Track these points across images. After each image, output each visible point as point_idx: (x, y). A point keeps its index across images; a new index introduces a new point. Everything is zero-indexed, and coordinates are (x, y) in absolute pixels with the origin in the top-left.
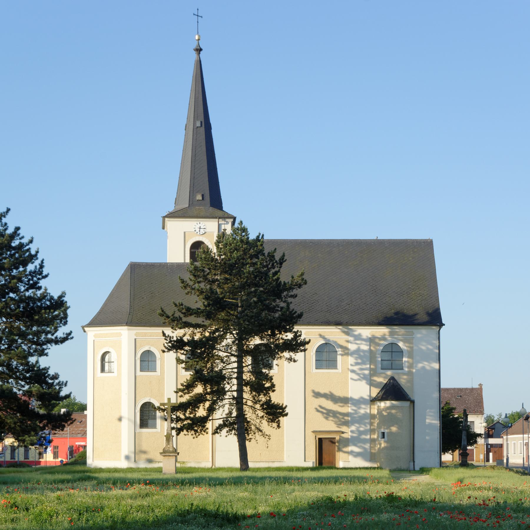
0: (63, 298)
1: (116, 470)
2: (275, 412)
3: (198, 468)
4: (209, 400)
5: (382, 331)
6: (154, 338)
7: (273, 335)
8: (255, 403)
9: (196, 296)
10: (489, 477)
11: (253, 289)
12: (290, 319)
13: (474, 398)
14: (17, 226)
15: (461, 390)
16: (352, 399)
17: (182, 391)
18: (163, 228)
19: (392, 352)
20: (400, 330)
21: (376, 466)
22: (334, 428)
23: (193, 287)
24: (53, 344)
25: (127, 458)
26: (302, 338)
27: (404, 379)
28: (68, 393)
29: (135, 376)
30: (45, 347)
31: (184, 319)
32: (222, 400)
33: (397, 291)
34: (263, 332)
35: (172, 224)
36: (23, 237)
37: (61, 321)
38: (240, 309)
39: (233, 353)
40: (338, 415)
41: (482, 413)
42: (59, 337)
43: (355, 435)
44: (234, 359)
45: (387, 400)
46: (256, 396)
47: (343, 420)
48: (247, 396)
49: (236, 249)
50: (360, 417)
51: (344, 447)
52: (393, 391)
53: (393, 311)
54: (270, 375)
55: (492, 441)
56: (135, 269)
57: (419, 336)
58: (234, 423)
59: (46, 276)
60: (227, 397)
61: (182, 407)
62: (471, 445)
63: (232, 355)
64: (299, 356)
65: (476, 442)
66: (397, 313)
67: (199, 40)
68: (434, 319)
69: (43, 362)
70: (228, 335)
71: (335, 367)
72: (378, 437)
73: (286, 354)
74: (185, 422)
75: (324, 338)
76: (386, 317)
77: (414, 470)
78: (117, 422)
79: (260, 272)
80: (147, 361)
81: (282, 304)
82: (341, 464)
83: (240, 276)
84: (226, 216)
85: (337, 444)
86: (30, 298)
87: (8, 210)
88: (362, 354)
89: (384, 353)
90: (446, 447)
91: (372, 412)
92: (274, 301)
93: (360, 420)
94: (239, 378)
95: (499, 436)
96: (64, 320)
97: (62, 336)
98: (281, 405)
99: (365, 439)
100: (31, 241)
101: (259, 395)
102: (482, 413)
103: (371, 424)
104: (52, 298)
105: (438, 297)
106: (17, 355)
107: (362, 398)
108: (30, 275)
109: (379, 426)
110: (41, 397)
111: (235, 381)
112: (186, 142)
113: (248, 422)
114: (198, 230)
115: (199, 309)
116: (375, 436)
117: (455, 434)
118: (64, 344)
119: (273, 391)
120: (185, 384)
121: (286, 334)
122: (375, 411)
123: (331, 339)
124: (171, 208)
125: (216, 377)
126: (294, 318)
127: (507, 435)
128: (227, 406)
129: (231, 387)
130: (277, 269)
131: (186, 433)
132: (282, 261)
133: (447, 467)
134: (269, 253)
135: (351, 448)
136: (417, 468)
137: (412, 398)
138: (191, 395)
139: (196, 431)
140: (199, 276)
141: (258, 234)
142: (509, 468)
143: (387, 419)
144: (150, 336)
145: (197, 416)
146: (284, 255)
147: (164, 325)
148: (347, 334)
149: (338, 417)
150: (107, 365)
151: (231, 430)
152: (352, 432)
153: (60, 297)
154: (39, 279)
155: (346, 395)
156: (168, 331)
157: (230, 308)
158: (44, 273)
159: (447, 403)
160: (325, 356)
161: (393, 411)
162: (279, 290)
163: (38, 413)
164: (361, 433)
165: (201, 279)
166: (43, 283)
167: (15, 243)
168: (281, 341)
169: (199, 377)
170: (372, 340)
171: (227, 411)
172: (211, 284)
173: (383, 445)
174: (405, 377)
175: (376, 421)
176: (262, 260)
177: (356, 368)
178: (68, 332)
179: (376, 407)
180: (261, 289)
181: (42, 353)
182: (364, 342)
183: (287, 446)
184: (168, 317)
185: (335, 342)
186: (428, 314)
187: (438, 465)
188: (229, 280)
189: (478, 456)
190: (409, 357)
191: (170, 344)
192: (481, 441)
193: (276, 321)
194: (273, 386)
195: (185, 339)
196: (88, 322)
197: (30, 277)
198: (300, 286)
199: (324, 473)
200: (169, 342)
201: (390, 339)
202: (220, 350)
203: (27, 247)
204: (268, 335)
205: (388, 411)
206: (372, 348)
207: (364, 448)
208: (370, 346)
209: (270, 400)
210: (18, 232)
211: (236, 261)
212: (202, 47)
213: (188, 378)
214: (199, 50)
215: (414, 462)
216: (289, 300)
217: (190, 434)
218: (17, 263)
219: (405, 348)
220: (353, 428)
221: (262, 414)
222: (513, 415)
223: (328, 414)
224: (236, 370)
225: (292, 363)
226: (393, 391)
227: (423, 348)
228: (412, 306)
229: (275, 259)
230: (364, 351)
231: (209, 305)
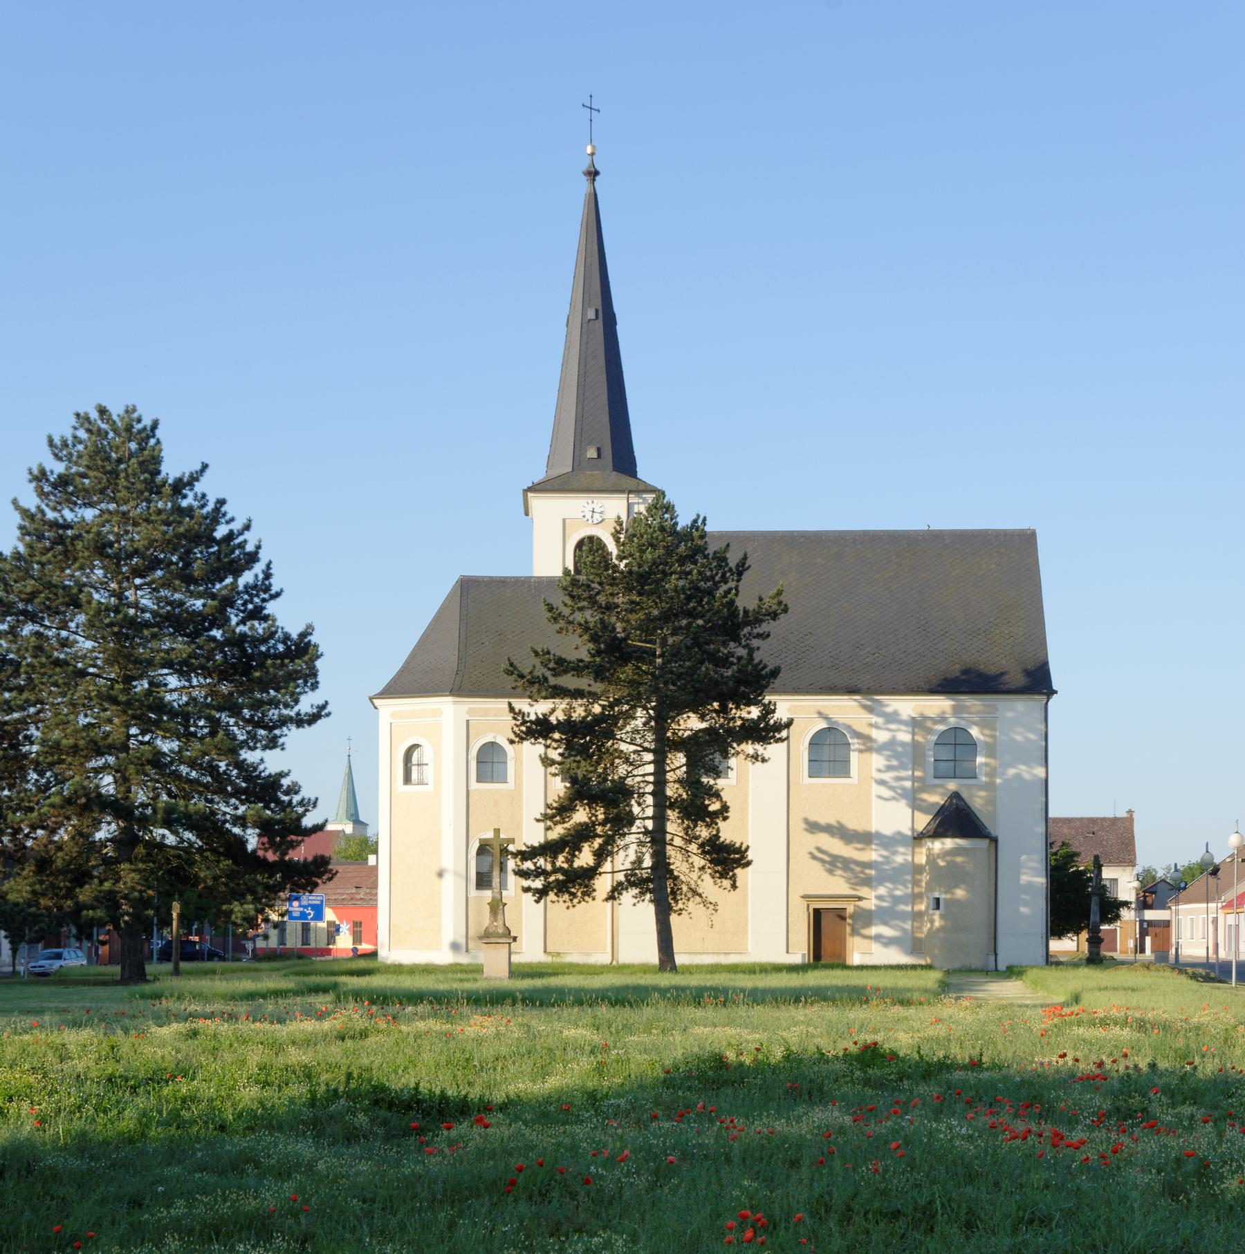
0: (309, 638)
1: (428, 970)
2: (727, 860)
3: (584, 965)
4: (600, 836)
5: (938, 705)
6: (493, 717)
7: (724, 710)
8: (690, 842)
9: (576, 636)
10: (1133, 990)
11: (684, 622)
12: (755, 682)
13: (1117, 837)
14: (221, 496)
15: (1093, 821)
16: (878, 835)
17: (551, 818)
18: (527, 514)
19: (957, 744)
20: (973, 703)
21: (923, 962)
22: (845, 889)
23: (571, 619)
24: (293, 727)
25: (455, 947)
26: (777, 716)
27: (980, 797)
28: (320, 821)
29: (468, 791)
30: (277, 732)
31: (553, 681)
32: (624, 835)
33: (965, 625)
34: (704, 704)
35: (542, 504)
36: (232, 520)
37: (306, 682)
38: (659, 661)
39: (646, 745)
40: (852, 866)
41: (1132, 863)
42: (303, 712)
43: (885, 904)
44: (649, 757)
45: (946, 836)
46: (689, 827)
47: (862, 875)
48: (674, 827)
49: (651, 545)
50: (894, 869)
51: (863, 928)
52: (957, 820)
53: (958, 666)
54: (719, 787)
55: (1150, 915)
56: (468, 587)
57: (1009, 715)
58: (648, 880)
59: (278, 595)
60: (634, 829)
61: (550, 849)
62: (1110, 921)
63: (646, 750)
64: (774, 751)
65: (1117, 917)
66: (966, 672)
67: (593, 154)
68: (1038, 682)
69: (270, 762)
70: (640, 712)
71: (845, 773)
72: (927, 908)
73: (749, 748)
74: (552, 878)
75: (827, 718)
76: (945, 679)
77: (996, 970)
78: (434, 878)
79: (697, 589)
80: (489, 762)
81: (741, 652)
82: (856, 959)
83: (659, 597)
84: (642, 487)
85: (849, 921)
86: (243, 636)
87: (205, 467)
88: (900, 749)
89: (940, 747)
90: (1057, 928)
91: (916, 861)
92: (725, 644)
93: (895, 876)
94: (659, 793)
95: (1163, 906)
96: (310, 677)
97: (309, 710)
98: (737, 845)
99: (904, 912)
100: (247, 527)
101: (696, 826)
102: (1132, 863)
103: (916, 883)
104: (287, 637)
105: (1045, 639)
106: (216, 747)
107: (899, 833)
108: (247, 592)
109: (930, 888)
110: (266, 828)
111: (649, 800)
112: (567, 348)
113: (676, 878)
114: (589, 515)
115: (581, 661)
116: (923, 907)
117: (1076, 900)
118: (314, 726)
119: (725, 819)
120: (555, 805)
121: (748, 709)
122: (921, 859)
123: (841, 721)
124: (539, 475)
125: (610, 790)
126: (763, 678)
127: (1177, 903)
128: (633, 847)
129: (643, 810)
130: (732, 584)
131: (555, 898)
132: (742, 568)
133: (1058, 964)
134: (715, 553)
135: (874, 930)
136: (1002, 966)
137: (993, 834)
138: (567, 825)
139: (574, 895)
140: (579, 598)
141: (694, 517)
142: (1180, 967)
143: (946, 875)
144: (496, 715)
145: (576, 865)
146: (745, 558)
147: (513, 693)
148: (870, 710)
149: (852, 870)
150: (414, 769)
151: (642, 893)
152: (879, 898)
153: (303, 635)
154: (264, 600)
155: (867, 829)
156: (522, 704)
157: (640, 659)
158: (274, 589)
159: (1064, 844)
160: (826, 752)
161: (959, 859)
162: (733, 624)
163: (265, 859)
164: (897, 900)
165: (585, 603)
166: (271, 608)
167: (221, 532)
168: (739, 723)
169: (581, 792)
170: (917, 724)
171: (632, 857)
172: (603, 613)
173: (937, 924)
174: (982, 793)
175: (925, 878)
176: (703, 566)
177: (887, 776)
178: (321, 702)
179: (924, 850)
180: (700, 622)
181: (272, 743)
182: (903, 728)
183: (749, 924)
184: (522, 676)
185: (849, 727)
186: (1028, 673)
187: (1042, 960)
188: (638, 604)
189: (1124, 941)
190: (987, 756)
191: (524, 728)
192: (1127, 915)
193: (726, 683)
194: (725, 808)
195: (553, 719)
196: (379, 690)
197: (246, 597)
198: (774, 616)
199: (815, 979)
200: (522, 724)
201: (953, 721)
202: (621, 739)
203: (241, 539)
204: (715, 711)
205: (948, 858)
206: (919, 738)
207: (904, 930)
208: (913, 734)
209: (717, 836)
210: (223, 509)
211: (650, 567)
212: (598, 168)
213: (562, 795)
214: (593, 174)
215: (996, 955)
216: (755, 643)
217: (561, 900)
218: (219, 569)
219: (982, 738)
220: (882, 891)
221: (703, 862)
222: (1191, 869)
223: (834, 863)
224: (651, 779)
225: (759, 764)
226: (957, 820)
227: (1018, 738)
228: (993, 660)
229: (727, 564)
230: (903, 744)
231: (599, 653)
